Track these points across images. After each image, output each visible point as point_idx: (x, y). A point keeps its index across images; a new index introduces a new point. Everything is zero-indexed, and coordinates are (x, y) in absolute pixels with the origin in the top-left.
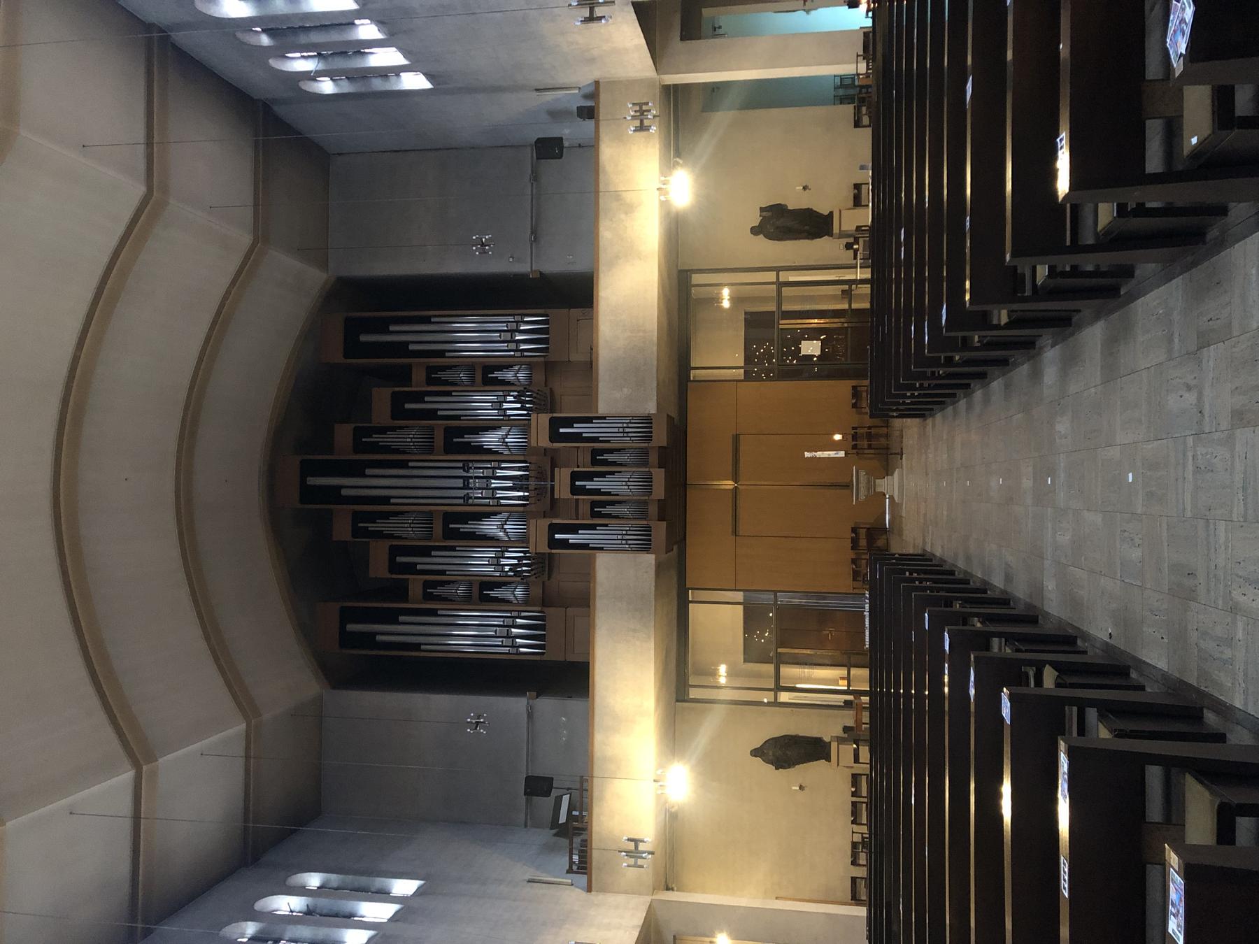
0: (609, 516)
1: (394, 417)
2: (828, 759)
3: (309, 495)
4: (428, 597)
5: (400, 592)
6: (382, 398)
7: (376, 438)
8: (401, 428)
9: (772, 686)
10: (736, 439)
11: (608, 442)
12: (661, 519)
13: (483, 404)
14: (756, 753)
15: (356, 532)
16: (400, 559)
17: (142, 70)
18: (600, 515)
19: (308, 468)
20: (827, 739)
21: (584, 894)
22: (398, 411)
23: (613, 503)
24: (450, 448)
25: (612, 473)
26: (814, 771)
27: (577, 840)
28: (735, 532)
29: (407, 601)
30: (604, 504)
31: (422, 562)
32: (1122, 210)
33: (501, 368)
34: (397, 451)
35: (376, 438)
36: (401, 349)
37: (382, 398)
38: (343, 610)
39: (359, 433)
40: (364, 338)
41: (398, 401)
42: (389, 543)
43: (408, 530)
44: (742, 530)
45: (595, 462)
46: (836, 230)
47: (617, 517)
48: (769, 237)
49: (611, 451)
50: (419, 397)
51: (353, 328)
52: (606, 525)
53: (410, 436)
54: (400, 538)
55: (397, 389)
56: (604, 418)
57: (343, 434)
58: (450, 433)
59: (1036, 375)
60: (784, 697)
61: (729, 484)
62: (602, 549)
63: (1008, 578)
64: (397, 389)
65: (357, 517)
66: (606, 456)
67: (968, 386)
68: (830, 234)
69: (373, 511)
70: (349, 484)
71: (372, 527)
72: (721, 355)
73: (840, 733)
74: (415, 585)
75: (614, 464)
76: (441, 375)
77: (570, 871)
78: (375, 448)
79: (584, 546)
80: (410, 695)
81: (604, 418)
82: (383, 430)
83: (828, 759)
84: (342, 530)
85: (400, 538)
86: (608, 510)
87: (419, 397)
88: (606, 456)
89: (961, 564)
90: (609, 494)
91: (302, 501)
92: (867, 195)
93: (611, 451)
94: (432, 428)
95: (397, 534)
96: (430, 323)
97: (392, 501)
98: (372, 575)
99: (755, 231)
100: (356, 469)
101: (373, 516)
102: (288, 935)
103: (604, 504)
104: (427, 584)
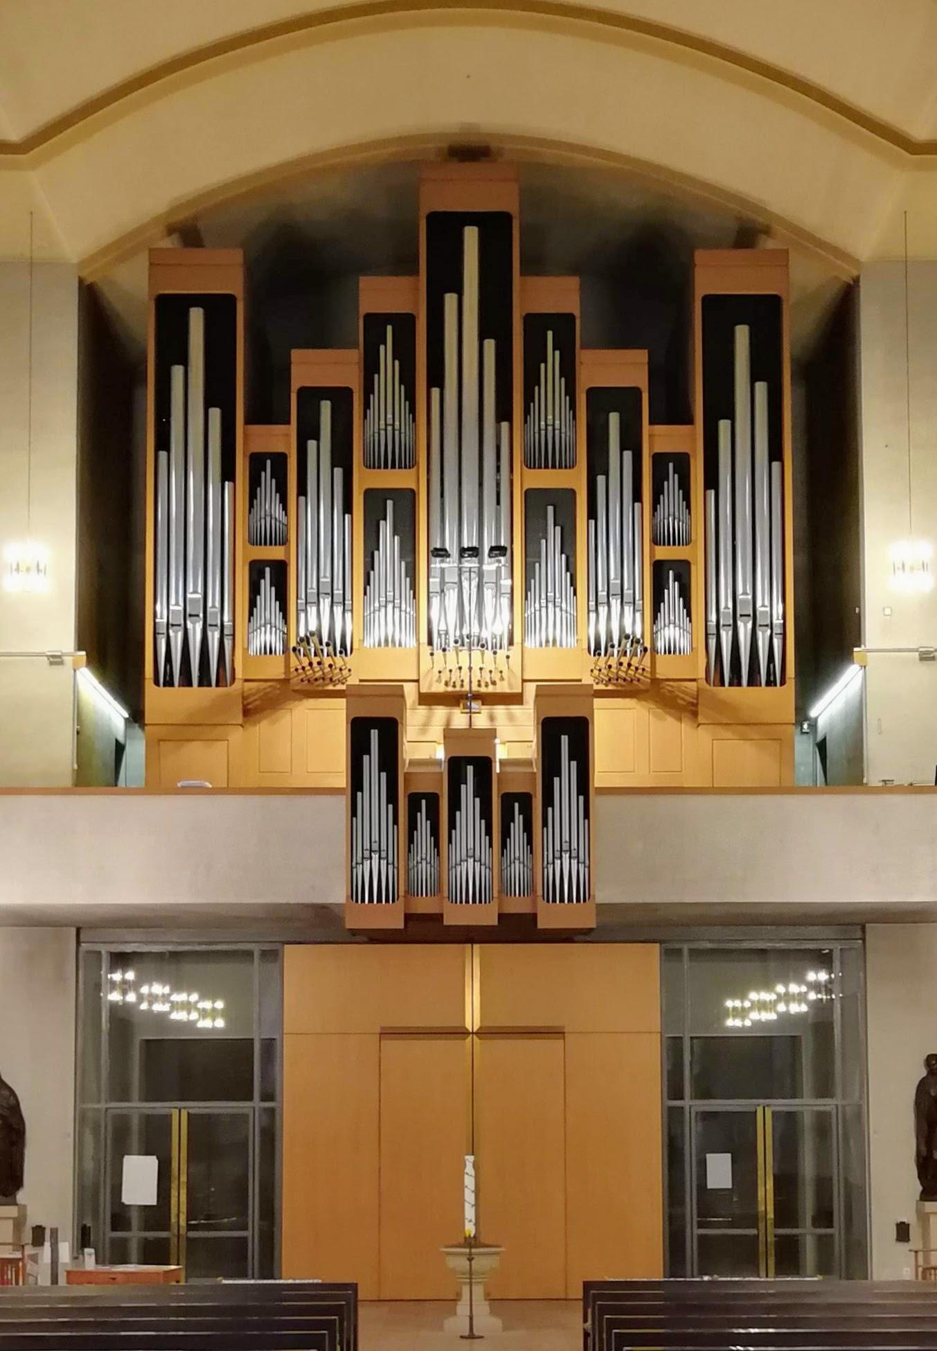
0: (412, 826)
1: (591, 392)
3: (446, 229)
4: (257, 462)
5: (266, 410)
6: (626, 369)
8: (573, 406)
10: (556, 1033)
11: (545, 824)
12: (408, 917)
15: (376, 323)
16: (326, 407)
19: (495, 228)
20: (21, 1196)
22: (602, 400)
23: (435, 832)
25: (489, 832)
28: (388, 1033)
29: (249, 421)
31: (321, 449)
34: (529, 398)
35: (553, 358)
36: (721, 405)
38: (230, 300)
39: (563, 323)
40: (742, 334)
41: (625, 399)
42: (354, 380)
43: (381, 417)
45: (508, 799)
49: (528, 828)
50: (631, 441)
51: (764, 313)
52: (396, 822)
53: (556, 415)
54: (367, 405)
56: (587, 816)
57: (557, 294)
61: (473, 1018)
65: (404, 323)
69: (412, 349)
71: (386, 352)
73: (33, 1219)
75: (506, 833)
78: (535, 357)
80: (74, 432)
81: (587, 816)
82: (568, 371)
84: (382, 294)
85: (367, 405)
86: (424, 825)
87: (631, 441)
88: (519, 819)
90: (452, 825)
91: (433, 218)
93: (528, 828)
95: (374, 399)
98: (296, 354)
100: (494, 321)
101: (404, 354)
104: (280, 461)
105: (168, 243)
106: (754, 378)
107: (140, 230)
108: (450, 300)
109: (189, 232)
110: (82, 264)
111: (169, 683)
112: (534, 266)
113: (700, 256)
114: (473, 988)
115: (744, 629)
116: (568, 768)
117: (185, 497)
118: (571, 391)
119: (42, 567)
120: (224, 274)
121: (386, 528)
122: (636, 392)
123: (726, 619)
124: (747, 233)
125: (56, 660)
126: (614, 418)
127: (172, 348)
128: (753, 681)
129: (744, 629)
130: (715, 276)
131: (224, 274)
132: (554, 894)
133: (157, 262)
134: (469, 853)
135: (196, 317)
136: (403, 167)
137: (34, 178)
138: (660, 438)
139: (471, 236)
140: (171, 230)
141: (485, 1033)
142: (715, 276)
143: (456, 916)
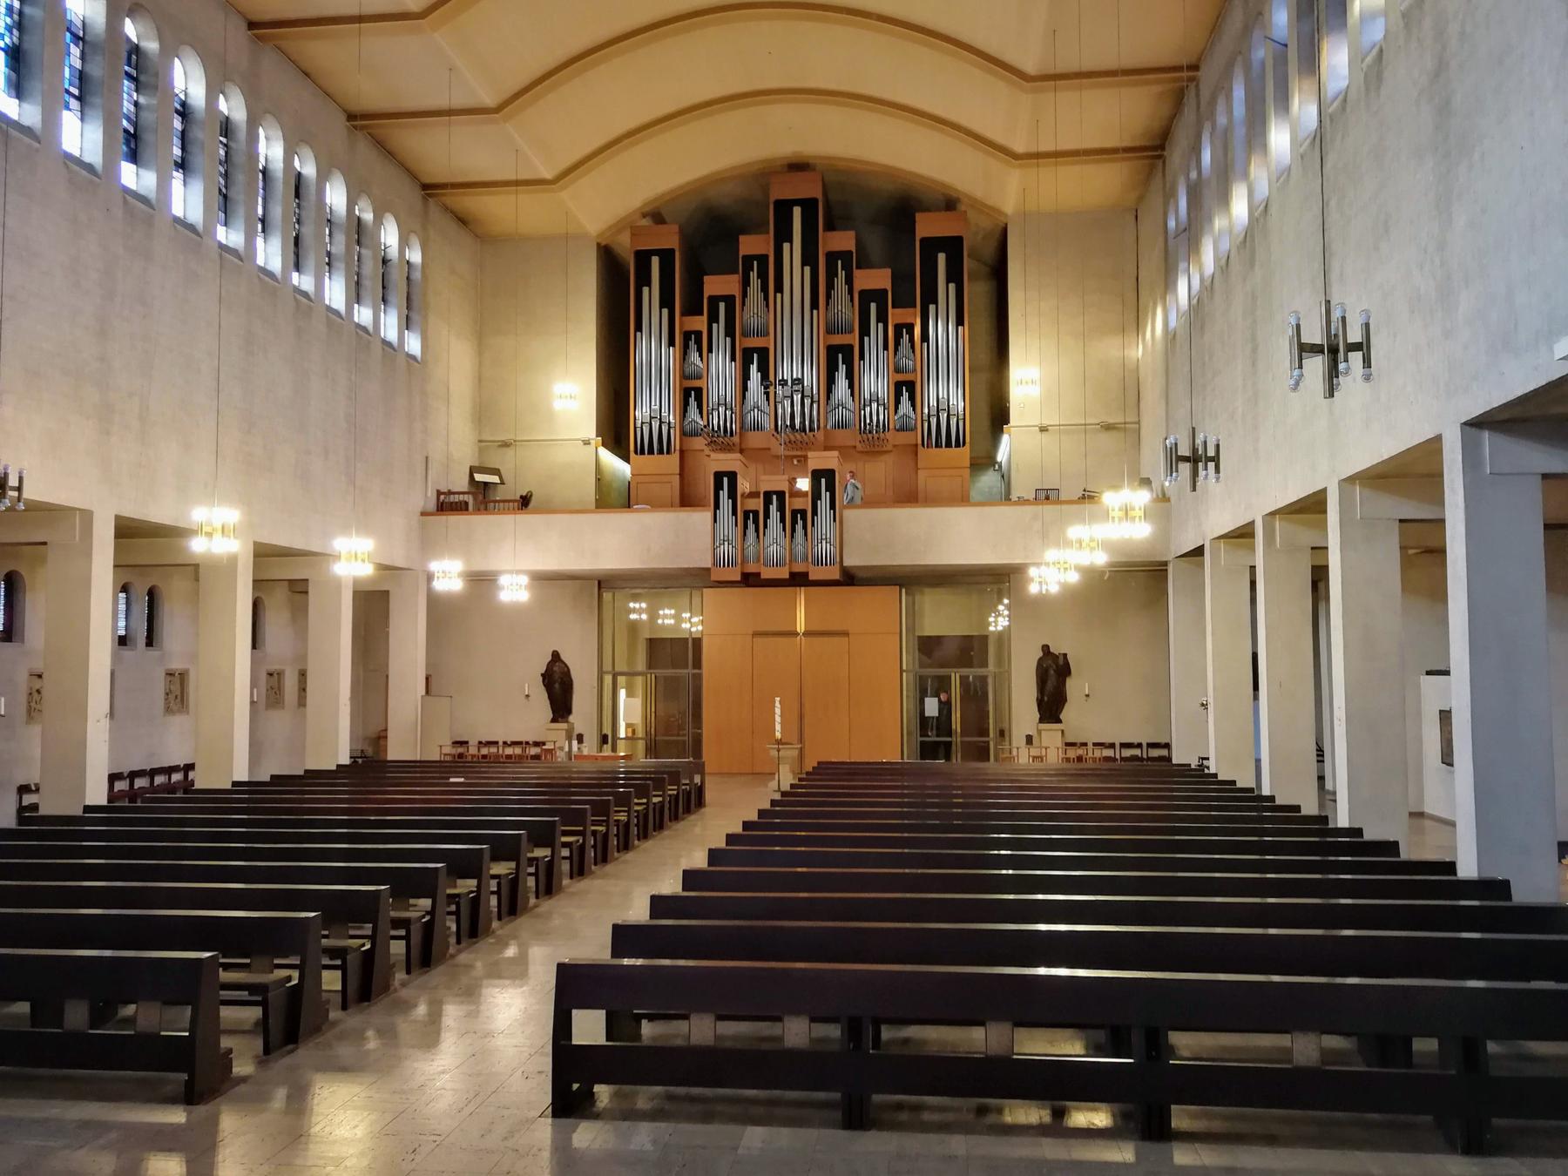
1: (862, 293)
2: (553, 721)
3: (783, 208)
4: (687, 336)
5: (693, 309)
7: (841, 274)
9: (617, 669)
10: (846, 634)
12: (792, 574)
13: (875, 382)
14: (556, 656)
15: (748, 260)
16: (722, 306)
17: (1137, 143)
18: (746, 518)
19: (809, 206)
20: (571, 718)
22: (867, 296)
23: (757, 530)
24: (832, 352)
27: (469, 499)
28: (756, 634)
29: (683, 314)
30: (756, 522)
31: (719, 328)
33: (912, 399)
34: (828, 296)
35: (841, 274)
36: (930, 297)
37: (878, 279)
39: (845, 256)
40: (942, 257)
43: (752, 312)
44: (758, 640)
45: (794, 513)
46: (1043, 726)
49: (805, 527)
50: (882, 318)
51: (953, 246)
53: (844, 308)
57: (843, 241)
58: (847, 350)
60: (608, 679)
61: (801, 626)
65: (762, 259)
66: (800, 522)
68: (1041, 721)
69: (769, 274)
70: (794, 251)
71: (754, 275)
72: (941, 616)
73: (577, 731)
74: (700, 323)
75: (793, 530)
77: (439, 493)
78: (831, 275)
79: (717, 506)
82: (849, 281)
83: (553, 721)
87: (882, 318)
88: (800, 522)
90: (765, 526)
91: (778, 203)
92: (1038, 765)
93: (805, 527)
94: (851, 331)
99: (1046, 648)
100: (809, 258)
101: (763, 276)
102: (364, 251)
103: (756, 522)
104: (699, 334)
105: (645, 222)
106: (948, 281)
107: (629, 216)
108: (786, 246)
109: (657, 216)
110: (599, 236)
111: (642, 453)
112: (830, 227)
113: (919, 216)
114: (801, 611)
115: (943, 417)
116: (825, 496)
117: (651, 352)
118: (851, 292)
119: (1316, 366)
120: (669, 239)
121: (754, 368)
122: (885, 291)
123: (934, 412)
124: (951, 204)
125: (587, 443)
126: (873, 306)
127: (644, 279)
128: (949, 445)
129: (943, 417)
130: (928, 226)
131: (669, 239)
132: (818, 562)
133: (636, 232)
134: (774, 540)
135: (655, 261)
136: (764, 174)
137: (564, 195)
138: (895, 316)
139: (797, 211)
140: (644, 216)
141: (806, 634)
142: (928, 226)
143: (767, 573)
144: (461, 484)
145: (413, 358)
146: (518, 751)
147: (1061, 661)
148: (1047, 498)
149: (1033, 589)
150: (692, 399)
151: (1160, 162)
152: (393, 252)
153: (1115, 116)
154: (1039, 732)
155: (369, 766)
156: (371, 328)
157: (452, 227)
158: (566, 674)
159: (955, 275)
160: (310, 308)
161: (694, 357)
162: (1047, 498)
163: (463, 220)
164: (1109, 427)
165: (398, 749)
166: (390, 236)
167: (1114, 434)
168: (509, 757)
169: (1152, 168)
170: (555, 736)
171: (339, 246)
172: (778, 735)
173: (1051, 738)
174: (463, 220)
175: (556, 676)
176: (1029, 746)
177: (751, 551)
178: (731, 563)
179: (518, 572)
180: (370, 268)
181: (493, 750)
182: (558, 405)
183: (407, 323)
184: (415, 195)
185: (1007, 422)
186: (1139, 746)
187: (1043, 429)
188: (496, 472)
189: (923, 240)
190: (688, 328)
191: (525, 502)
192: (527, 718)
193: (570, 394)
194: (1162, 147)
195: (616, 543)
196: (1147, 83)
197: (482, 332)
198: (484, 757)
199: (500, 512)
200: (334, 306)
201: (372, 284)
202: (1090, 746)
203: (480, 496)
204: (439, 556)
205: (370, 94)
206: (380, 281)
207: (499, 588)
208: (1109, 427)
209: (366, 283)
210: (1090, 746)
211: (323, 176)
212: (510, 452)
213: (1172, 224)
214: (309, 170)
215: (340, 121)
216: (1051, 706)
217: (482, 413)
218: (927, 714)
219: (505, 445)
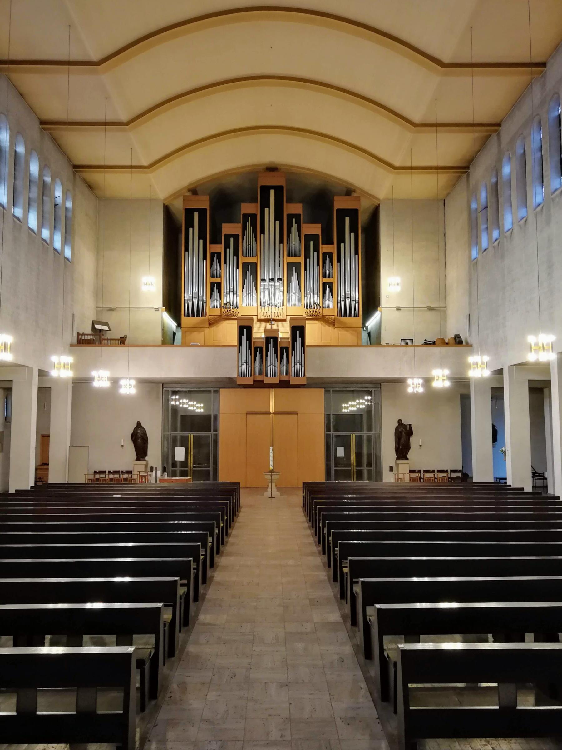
0: (256, 356)
1: (305, 236)
3: (265, 190)
4: (213, 255)
5: (215, 240)
6: (315, 229)
8: (300, 240)
10: (296, 413)
11: (292, 355)
12: (254, 381)
14: (139, 424)
15: (246, 216)
16: (232, 240)
17: (456, 165)
19: (279, 190)
20: (147, 458)
21: (69, 343)
22: (308, 238)
23: (262, 357)
25: (277, 357)
26: (130, 450)
28: (249, 413)
29: (210, 243)
30: (261, 353)
32: (346, 573)
34: (288, 237)
35: (295, 226)
36: (341, 240)
39: (297, 217)
40: (347, 220)
41: (315, 238)
42: (240, 232)
43: (247, 242)
44: (249, 417)
45: (282, 349)
46: (399, 462)
47: (255, 360)
48: (397, 428)
49: (288, 356)
50: (316, 249)
51: (353, 214)
52: (251, 355)
53: (296, 242)
54: (243, 239)
55: (320, 237)
56: (304, 353)
57: (295, 208)
59: (312, 554)
62: (239, 352)
63: (233, 544)
64: (320, 237)
65: (254, 216)
67: (313, 528)
68: (398, 458)
69: (256, 224)
71: (249, 224)
74: (219, 248)
75: (281, 358)
76: (328, 260)
78: (290, 226)
81: (304, 353)
82: (299, 230)
84: (248, 208)
85: (243, 239)
87: (316, 249)
88: (285, 354)
89: (237, 524)
90: (267, 356)
93: (288, 356)
96: (355, 254)
97: (262, 235)
98: (224, 225)
99: (400, 422)
100: (279, 216)
101: (254, 225)
103: (261, 353)
104: (219, 254)
105: (188, 194)
106: (351, 232)
109: (194, 191)
110: (165, 200)
111: (188, 316)
112: (290, 201)
114: (272, 401)
115: (348, 301)
116: (299, 340)
117: (193, 264)
118: (300, 235)
120: (204, 203)
121: (248, 273)
122: (318, 235)
123: (343, 299)
124: (349, 192)
125: (157, 310)
126: (312, 243)
127: (189, 223)
129: (348, 301)
130: (340, 203)
131: (204, 203)
132: (295, 375)
133: (185, 199)
135: (196, 215)
138: (324, 248)
139: (272, 192)
141: (275, 413)
142: (340, 203)
143: (267, 381)
144: (89, 330)
145: (68, 259)
146: (116, 476)
147: (408, 429)
148: (407, 344)
149: (410, 390)
150: (215, 289)
151: (465, 175)
152: (59, 201)
153: (450, 148)
154: (397, 465)
155: (42, 486)
156: (48, 241)
157: (86, 190)
158: (145, 434)
159: (354, 229)
160: (21, 226)
161: (216, 266)
162: (407, 344)
163: (91, 187)
164: (431, 309)
165: (55, 477)
166: (58, 193)
167: (433, 312)
168: (111, 480)
169: (459, 178)
170: (139, 468)
171: (35, 193)
172: (271, 467)
173: (404, 467)
174: (91, 187)
175: (139, 435)
176: (392, 474)
177: (259, 368)
178: (248, 375)
179: (130, 379)
180: (48, 207)
181: (102, 475)
182: (145, 289)
183: (65, 241)
184: (70, 170)
185: (379, 305)
186: (447, 471)
187: (398, 309)
188: (106, 324)
189: (338, 210)
190: (213, 251)
191: (122, 341)
192: (123, 458)
193: (150, 283)
194: (468, 168)
195: (178, 365)
196: (474, 131)
197: (100, 248)
198: (97, 479)
199: (107, 345)
200: (31, 227)
201: (49, 216)
202: (422, 472)
203: (94, 338)
204: (96, 367)
205: (55, 110)
206: (55, 217)
207: (121, 387)
208: (431, 309)
209: (47, 216)
210: (422, 472)
211: (28, 152)
212: (114, 313)
213: (474, 206)
214: (21, 149)
215: (37, 126)
216: (402, 451)
217: (100, 292)
218: (183, 449)
219: (112, 309)
